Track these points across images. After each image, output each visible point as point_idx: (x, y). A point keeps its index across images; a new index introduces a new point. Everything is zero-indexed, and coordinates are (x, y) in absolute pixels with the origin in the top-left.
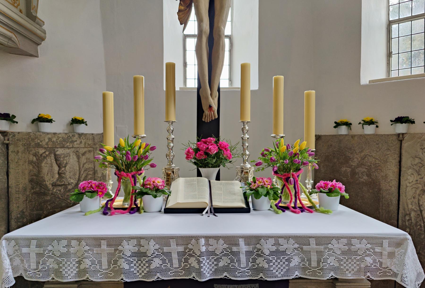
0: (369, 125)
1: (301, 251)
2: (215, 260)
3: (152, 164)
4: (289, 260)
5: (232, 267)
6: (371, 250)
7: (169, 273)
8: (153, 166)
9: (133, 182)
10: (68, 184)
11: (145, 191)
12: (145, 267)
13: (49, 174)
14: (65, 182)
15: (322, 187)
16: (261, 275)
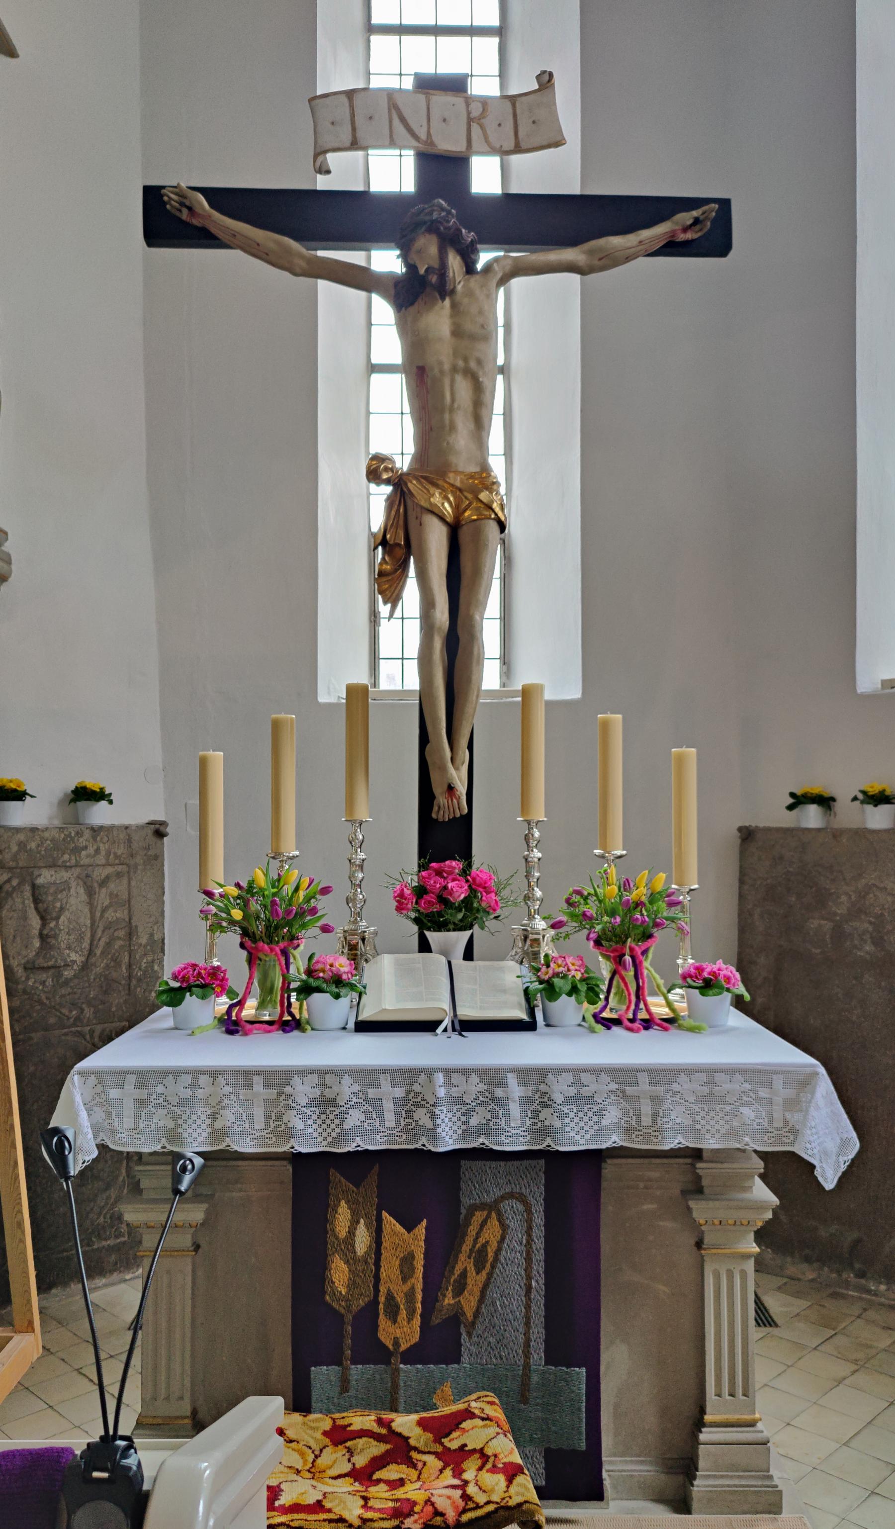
0: (876, 806)
1: (621, 1095)
2: (463, 1114)
3: (325, 925)
4: (600, 1114)
5: (495, 1127)
6: (751, 1094)
7: (378, 1137)
9: (284, 962)
10: (64, 966)
11: (313, 983)
12: (333, 1126)
13: (18, 940)
14: (56, 961)
15: (690, 976)
16: (549, 1141)
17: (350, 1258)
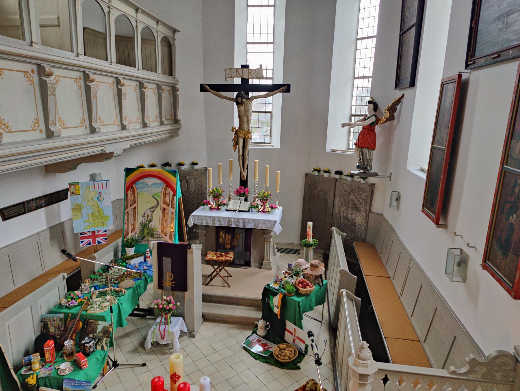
4: (251, 224)
8: (223, 197)
17: (222, 238)
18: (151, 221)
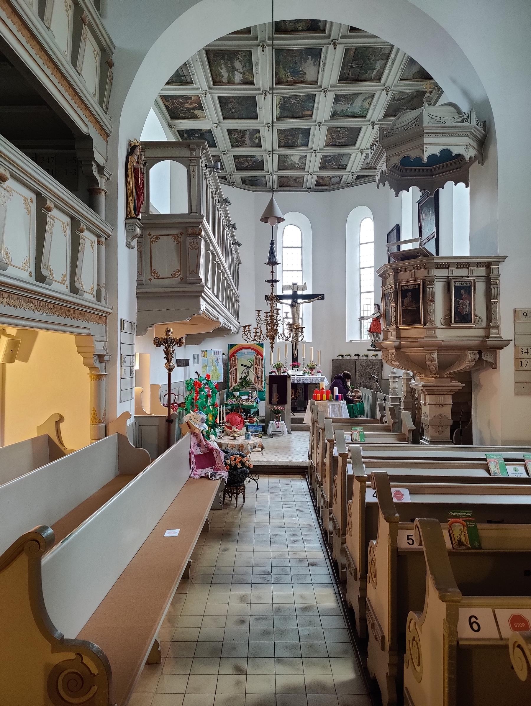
18: (247, 376)
